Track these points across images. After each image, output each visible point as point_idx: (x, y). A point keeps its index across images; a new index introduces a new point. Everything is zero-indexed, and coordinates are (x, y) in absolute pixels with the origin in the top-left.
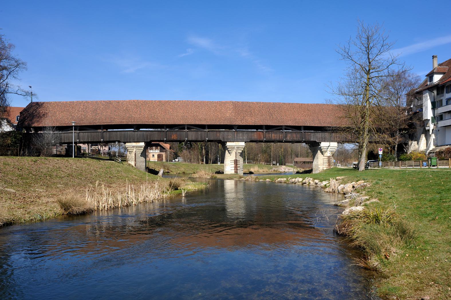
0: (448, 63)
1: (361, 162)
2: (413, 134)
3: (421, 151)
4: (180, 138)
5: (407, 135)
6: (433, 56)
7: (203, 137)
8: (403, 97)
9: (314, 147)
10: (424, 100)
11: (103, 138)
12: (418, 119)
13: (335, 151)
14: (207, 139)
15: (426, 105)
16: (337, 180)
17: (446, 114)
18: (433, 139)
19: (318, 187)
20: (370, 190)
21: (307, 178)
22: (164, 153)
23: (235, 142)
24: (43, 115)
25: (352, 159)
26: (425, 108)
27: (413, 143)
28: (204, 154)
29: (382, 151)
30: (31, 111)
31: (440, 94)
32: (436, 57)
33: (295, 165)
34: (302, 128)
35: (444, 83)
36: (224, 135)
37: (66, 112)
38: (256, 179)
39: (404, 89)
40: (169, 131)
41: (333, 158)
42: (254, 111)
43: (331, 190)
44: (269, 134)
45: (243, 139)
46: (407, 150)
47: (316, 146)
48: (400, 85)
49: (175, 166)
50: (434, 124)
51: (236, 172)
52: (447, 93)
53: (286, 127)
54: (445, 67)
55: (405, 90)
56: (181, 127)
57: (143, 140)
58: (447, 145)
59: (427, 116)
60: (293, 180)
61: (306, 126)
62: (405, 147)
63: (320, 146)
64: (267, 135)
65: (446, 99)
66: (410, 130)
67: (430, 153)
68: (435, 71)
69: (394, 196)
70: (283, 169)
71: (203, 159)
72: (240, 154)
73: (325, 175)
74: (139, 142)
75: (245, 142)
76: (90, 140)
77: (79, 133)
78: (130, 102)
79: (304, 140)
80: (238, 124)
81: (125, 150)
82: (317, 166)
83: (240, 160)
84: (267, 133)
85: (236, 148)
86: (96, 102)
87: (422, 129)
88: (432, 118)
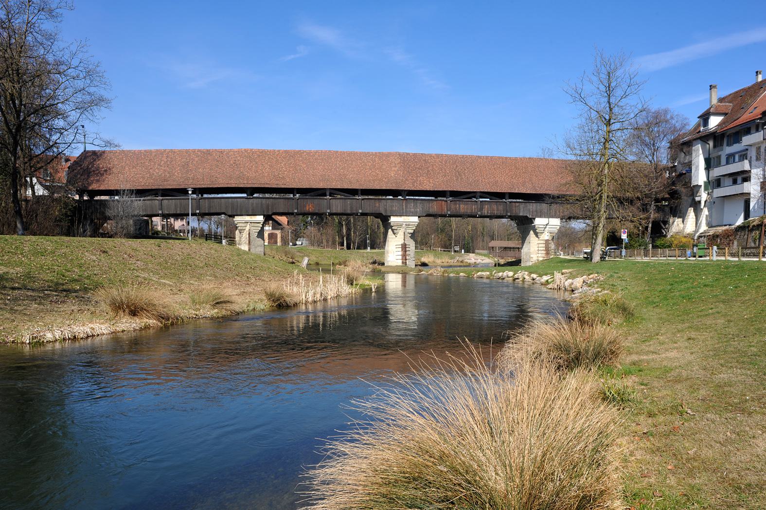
0: (732, 98)
1: (595, 250)
2: (676, 207)
3: (688, 233)
4: (319, 210)
5: (667, 209)
6: (710, 86)
7: (354, 208)
8: (662, 150)
9: (525, 225)
10: (694, 155)
11: (199, 209)
12: (684, 185)
13: (556, 232)
14: (360, 211)
15: (697, 164)
16: (562, 274)
17: (726, 177)
18: (705, 216)
19: (536, 284)
20: (602, 283)
21: (520, 271)
22: (280, 231)
23: (403, 217)
24: (104, 171)
25: (582, 244)
26: (695, 168)
27: (676, 220)
28: (345, 233)
29: (626, 234)
30: (85, 164)
31: (718, 146)
32: (715, 87)
33: (490, 253)
34: (507, 196)
35: (723, 130)
36: (386, 206)
37: (140, 167)
38: (443, 273)
39: (664, 137)
40: (302, 198)
41: (553, 243)
42: (433, 168)
43: (556, 287)
44: (456, 205)
45: (416, 212)
46: (667, 231)
47: (526, 224)
48: (658, 132)
49: (302, 253)
50: (708, 192)
51: (405, 263)
52: (728, 145)
53: (481, 194)
54: (727, 104)
55: (665, 138)
56: (320, 192)
57: (262, 212)
58: (725, 225)
59: (697, 180)
60: (500, 274)
61: (513, 193)
62: (664, 227)
63: (533, 225)
64: (453, 206)
65: (727, 155)
66: (671, 201)
67: (700, 237)
68: (711, 111)
69: (626, 288)
70: (471, 258)
71: (343, 242)
72: (410, 235)
73: (539, 268)
74: (242, 215)
75: (419, 217)
76: (178, 212)
77: (162, 200)
78: (239, 152)
79: (509, 214)
80: (408, 189)
81: (218, 226)
82: (528, 254)
83: (411, 245)
84: (452, 202)
85: (404, 226)
86: (187, 151)
87: (690, 200)
88: (705, 183)
